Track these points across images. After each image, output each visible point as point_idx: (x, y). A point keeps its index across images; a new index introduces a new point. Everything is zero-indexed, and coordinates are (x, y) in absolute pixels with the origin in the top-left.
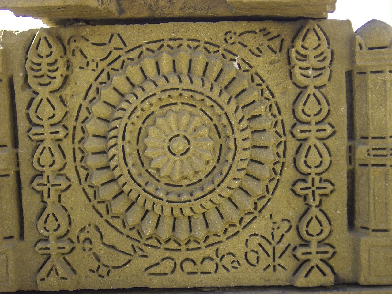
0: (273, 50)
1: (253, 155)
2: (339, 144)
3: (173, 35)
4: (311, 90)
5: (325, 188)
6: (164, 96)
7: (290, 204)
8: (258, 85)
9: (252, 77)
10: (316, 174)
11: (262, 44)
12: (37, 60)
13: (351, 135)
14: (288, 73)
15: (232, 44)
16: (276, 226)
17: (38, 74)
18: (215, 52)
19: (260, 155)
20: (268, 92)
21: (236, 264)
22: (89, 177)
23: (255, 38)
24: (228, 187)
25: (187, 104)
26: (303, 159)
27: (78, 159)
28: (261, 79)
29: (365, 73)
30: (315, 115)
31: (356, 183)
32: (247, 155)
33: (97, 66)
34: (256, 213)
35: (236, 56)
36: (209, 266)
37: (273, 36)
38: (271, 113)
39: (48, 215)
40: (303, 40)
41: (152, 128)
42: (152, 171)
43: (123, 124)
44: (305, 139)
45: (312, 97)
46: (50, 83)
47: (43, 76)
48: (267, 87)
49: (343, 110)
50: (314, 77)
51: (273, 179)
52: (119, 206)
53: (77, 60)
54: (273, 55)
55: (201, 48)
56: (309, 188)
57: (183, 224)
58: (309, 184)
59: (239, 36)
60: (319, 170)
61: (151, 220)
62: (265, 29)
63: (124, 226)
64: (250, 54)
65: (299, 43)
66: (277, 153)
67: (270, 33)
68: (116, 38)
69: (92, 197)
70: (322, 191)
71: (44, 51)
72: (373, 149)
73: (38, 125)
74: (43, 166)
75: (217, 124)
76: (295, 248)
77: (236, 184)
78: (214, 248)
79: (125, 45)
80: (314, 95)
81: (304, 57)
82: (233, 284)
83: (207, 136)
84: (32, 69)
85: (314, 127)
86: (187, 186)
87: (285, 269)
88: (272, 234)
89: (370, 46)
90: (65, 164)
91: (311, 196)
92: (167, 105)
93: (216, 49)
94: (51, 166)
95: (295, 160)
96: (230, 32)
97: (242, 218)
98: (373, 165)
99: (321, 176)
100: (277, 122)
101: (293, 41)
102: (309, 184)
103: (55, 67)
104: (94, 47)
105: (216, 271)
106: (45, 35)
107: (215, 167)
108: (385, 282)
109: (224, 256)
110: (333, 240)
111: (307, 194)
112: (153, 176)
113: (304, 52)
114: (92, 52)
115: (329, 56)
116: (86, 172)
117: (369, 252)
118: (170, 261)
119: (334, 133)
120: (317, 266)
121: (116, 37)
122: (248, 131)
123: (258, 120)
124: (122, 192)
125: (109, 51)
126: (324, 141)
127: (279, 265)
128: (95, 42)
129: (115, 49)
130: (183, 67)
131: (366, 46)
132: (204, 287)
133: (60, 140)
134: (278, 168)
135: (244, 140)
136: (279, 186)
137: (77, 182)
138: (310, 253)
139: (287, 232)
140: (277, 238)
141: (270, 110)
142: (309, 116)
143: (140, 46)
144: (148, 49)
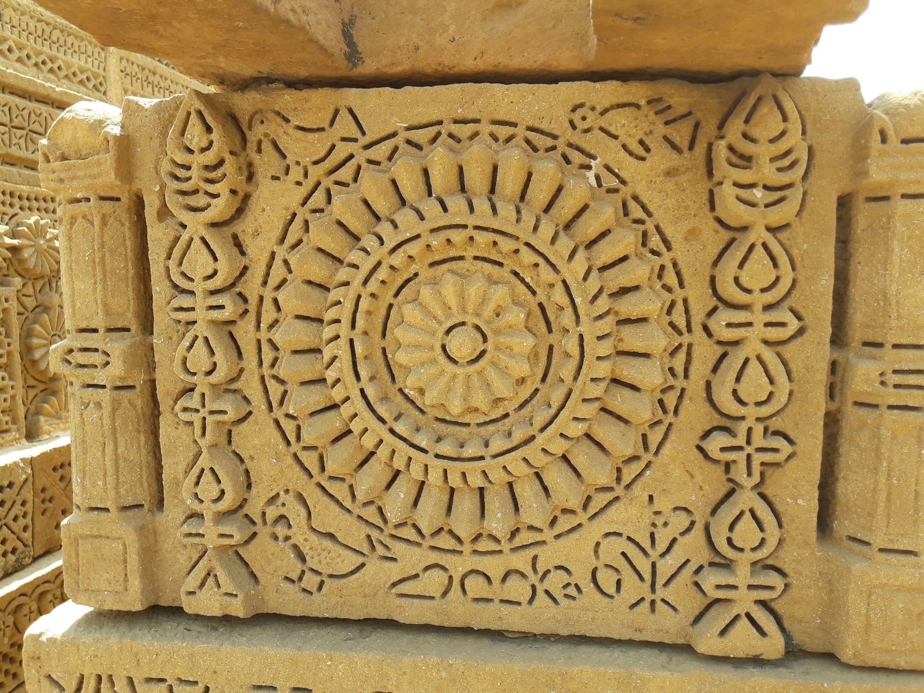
0: (674, 146)
1: (617, 372)
2: (814, 353)
3: (460, 113)
4: (759, 234)
5: (776, 450)
6: (436, 241)
7: (692, 476)
8: (636, 221)
9: (625, 205)
10: (758, 419)
11: (651, 132)
12: (181, 157)
13: (838, 339)
14: (705, 197)
15: (587, 131)
16: (660, 521)
17: (185, 186)
18: (548, 150)
19: (630, 370)
20: (658, 237)
21: (572, 591)
22: (287, 398)
23: (636, 119)
24: (562, 435)
25: (484, 259)
26: (730, 384)
27: (267, 362)
28: (644, 208)
29: (886, 198)
30: (763, 290)
31: (841, 441)
32: (603, 370)
33: (306, 175)
34: (619, 491)
35: (593, 157)
36: (517, 589)
37: (678, 114)
38: (661, 284)
39: (203, 470)
40: (747, 121)
41: (409, 306)
42: (411, 393)
43: (352, 296)
44: (736, 343)
45: (759, 249)
46: (209, 205)
47: (196, 192)
48: (657, 228)
49: (827, 282)
50: (766, 206)
51: (659, 422)
52: (339, 459)
53: (267, 163)
54: (675, 155)
55: (519, 140)
56: (740, 448)
57: (466, 504)
58: (741, 441)
59: (602, 114)
60: (765, 411)
61: (402, 491)
62: (659, 100)
63: (354, 496)
64: (623, 153)
65: (736, 127)
66: (671, 370)
67: (669, 107)
68: (344, 118)
69: (292, 438)
70: (768, 457)
71: (196, 139)
72: (895, 372)
73: (183, 291)
74: (195, 374)
75: (545, 304)
76: (701, 568)
77: (576, 430)
78: (530, 553)
79: (364, 133)
80: (764, 245)
81: (746, 161)
82: (564, 632)
83: (522, 326)
84: (177, 178)
85: (759, 317)
86: (479, 425)
87: (674, 609)
88: (652, 535)
89: (905, 136)
90: (242, 370)
91: (743, 465)
92: (444, 261)
93: (550, 142)
94: (209, 373)
95: (708, 385)
96: (582, 105)
97: (589, 498)
98: (891, 407)
99: (768, 422)
100: (673, 304)
101: (721, 126)
102: (741, 441)
103: (217, 174)
104: (300, 134)
105: (531, 601)
106: (198, 105)
107: (537, 390)
108: (902, 663)
109: (548, 571)
110: (785, 561)
111: (734, 462)
112: (412, 402)
113: (747, 148)
114: (304, 149)
115: (805, 157)
116: (281, 389)
117: (869, 597)
118: (441, 572)
119: (801, 332)
120: (748, 615)
121: (344, 114)
122: (610, 320)
123: (631, 297)
124: (350, 432)
125: (329, 144)
126: (779, 349)
127: (663, 600)
128: (302, 124)
129: (344, 139)
130: (477, 179)
131: (897, 136)
132: (507, 631)
133: (232, 322)
134: (671, 400)
135: (599, 338)
136: (672, 437)
137: (263, 407)
138: (735, 587)
139: (682, 534)
140: (661, 546)
141: (660, 277)
142: (749, 291)
143: (393, 135)
144: (409, 142)
